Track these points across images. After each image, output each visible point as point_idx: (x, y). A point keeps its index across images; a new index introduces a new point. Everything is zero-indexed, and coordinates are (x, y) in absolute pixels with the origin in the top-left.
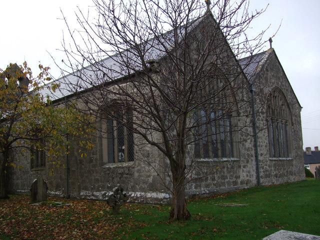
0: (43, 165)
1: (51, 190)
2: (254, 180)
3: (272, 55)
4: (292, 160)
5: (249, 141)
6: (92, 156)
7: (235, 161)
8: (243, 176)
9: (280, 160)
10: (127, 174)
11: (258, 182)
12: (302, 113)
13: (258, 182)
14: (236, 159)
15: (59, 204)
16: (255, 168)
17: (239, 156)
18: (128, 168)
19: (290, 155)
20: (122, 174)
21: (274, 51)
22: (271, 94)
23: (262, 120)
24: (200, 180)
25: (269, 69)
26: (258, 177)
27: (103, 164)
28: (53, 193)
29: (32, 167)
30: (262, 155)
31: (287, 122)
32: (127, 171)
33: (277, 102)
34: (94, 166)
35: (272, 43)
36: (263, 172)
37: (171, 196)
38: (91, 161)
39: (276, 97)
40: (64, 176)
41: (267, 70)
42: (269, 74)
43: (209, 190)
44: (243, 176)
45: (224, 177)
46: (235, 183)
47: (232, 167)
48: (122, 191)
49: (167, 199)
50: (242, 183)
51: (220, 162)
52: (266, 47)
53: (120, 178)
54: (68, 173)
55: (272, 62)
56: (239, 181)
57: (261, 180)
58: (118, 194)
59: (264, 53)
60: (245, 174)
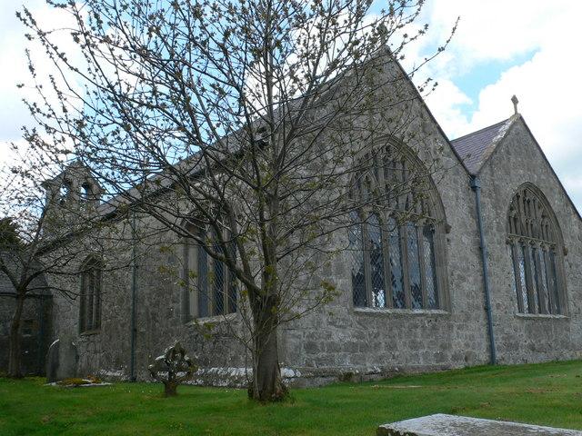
0: (98, 326)
1: (108, 369)
2: (483, 357)
3: (519, 121)
4: (566, 319)
5: (471, 279)
6: (171, 305)
7: (441, 315)
8: (458, 343)
9: (539, 319)
10: (226, 335)
11: (492, 356)
12: (490, 88)
13: (492, 356)
14: (442, 312)
15: (87, 383)
16: (484, 331)
17: (449, 307)
18: (228, 323)
19: (562, 309)
20: (217, 336)
21: (521, 118)
22: (518, 197)
23: (499, 243)
24: (365, 348)
25: (512, 150)
26: (491, 349)
27: (188, 319)
28: (110, 374)
29: (82, 329)
30: (498, 306)
31: (553, 249)
32: (225, 330)
33: (532, 209)
34: (174, 324)
35: (518, 105)
36: (503, 338)
37: (299, 374)
38: (170, 314)
39: (529, 202)
40: (128, 344)
41: (508, 153)
42: (513, 159)
43: (382, 369)
44: (458, 343)
45: (414, 346)
46: (441, 357)
47: (434, 328)
48: (183, 353)
49: (290, 378)
50: (455, 358)
51: (406, 317)
52: (506, 113)
53: (214, 343)
54: (134, 337)
55: (516, 139)
56: (449, 354)
57: (498, 355)
58: (174, 358)
59: (503, 123)
60: (462, 341)
